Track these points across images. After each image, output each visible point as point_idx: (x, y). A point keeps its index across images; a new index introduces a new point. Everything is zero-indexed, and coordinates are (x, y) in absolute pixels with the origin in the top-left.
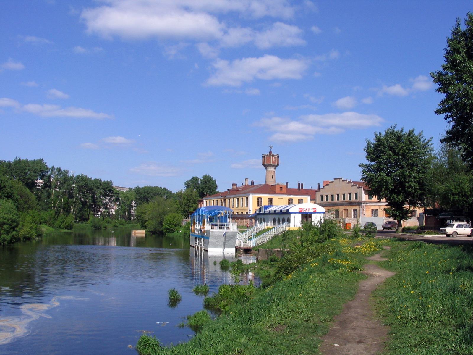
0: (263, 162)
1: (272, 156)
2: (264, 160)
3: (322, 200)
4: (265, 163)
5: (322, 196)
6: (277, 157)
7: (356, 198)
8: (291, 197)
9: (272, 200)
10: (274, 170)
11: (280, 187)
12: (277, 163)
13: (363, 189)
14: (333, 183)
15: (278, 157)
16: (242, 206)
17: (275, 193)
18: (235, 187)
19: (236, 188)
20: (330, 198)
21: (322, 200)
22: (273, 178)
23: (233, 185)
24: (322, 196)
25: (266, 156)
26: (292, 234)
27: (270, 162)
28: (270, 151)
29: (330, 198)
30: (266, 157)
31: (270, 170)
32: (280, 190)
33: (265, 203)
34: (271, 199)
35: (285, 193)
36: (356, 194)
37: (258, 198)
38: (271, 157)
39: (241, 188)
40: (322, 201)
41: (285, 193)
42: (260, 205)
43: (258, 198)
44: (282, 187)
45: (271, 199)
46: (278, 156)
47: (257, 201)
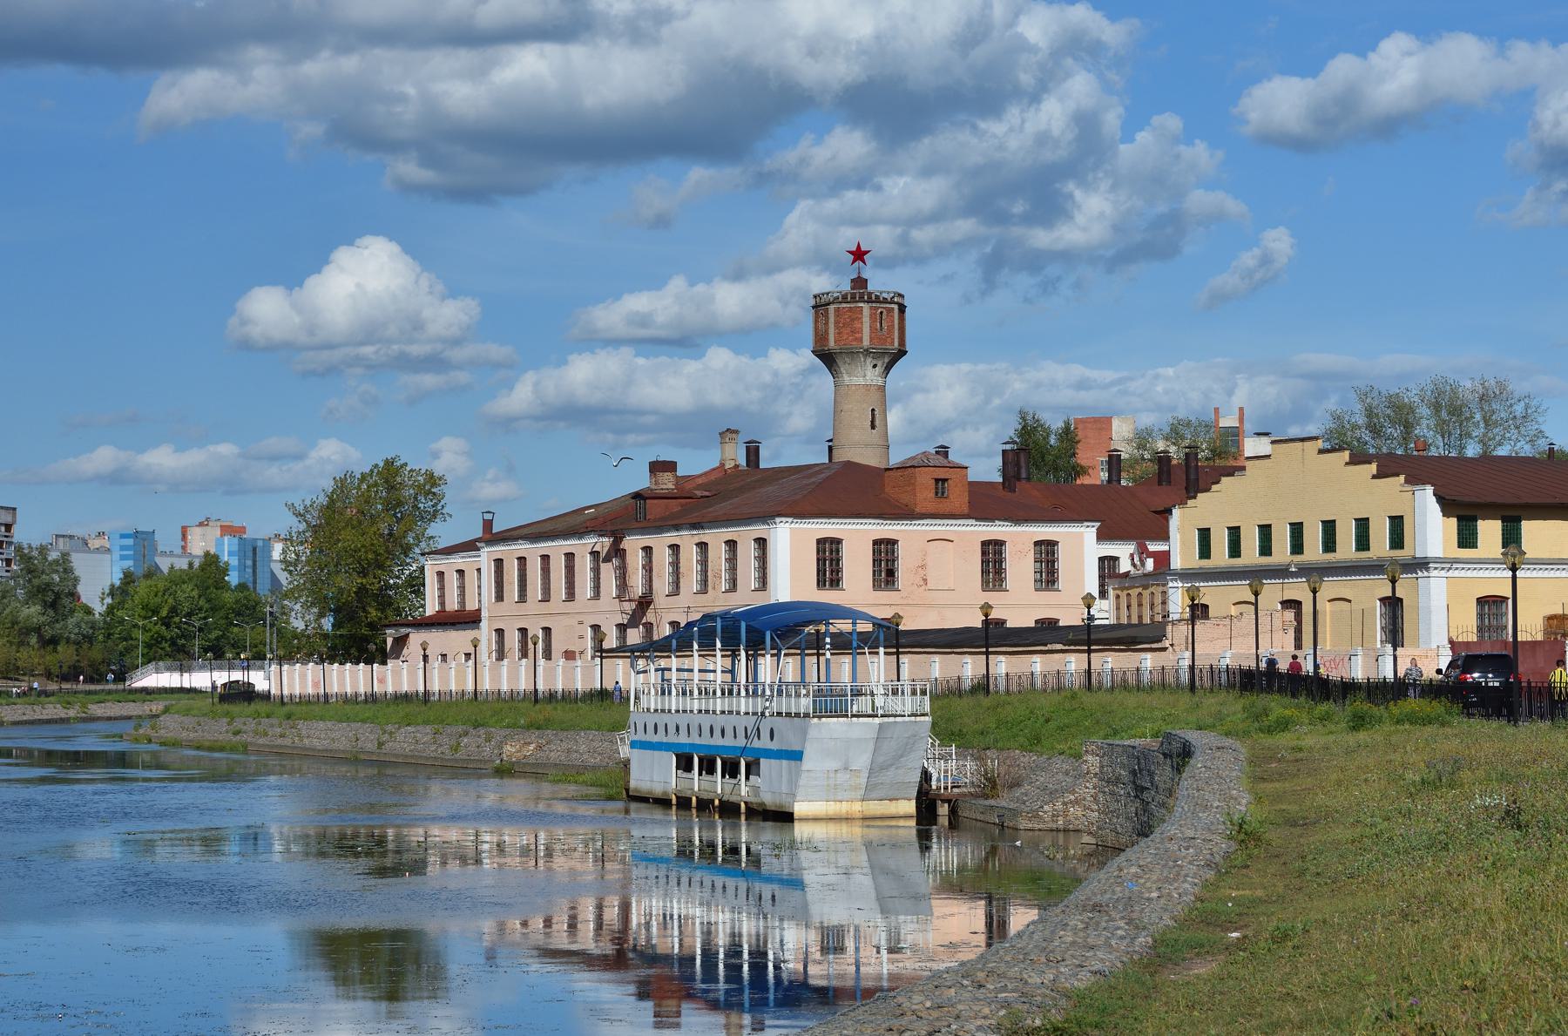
0: (820, 337)
1: (869, 301)
2: (827, 323)
3: (1205, 552)
4: (832, 343)
5: (1205, 534)
6: (896, 307)
7: (1397, 541)
8: (1265, 560)
9: (838, 551)
10: (880, 382)
11: (937, 480)
12: (896, 344)
13: (1440, 499)
14: (1266, 461)
15: (902, 309)
16: (546, 598)
17: (906, 513)
18: (667, 482)
19: (671, 486)
20: (1250, 542)
21: (1205, 552)
22: (873, 427)
23: (658, 467)
24: (1205, 534)
25: (835, 301)
26: (1076, 695)
27: (861, 340)
28: (855, 276)
29: (1250, 542)
30: (837, 310)
31: (861, 381)
32: (937, 493)
33: (1020, 566)
34: (836, 542)
35: (966, 510)
36: (1397, 523)
37: (821, 542)
38: (865, 307)
39: (700, 481)
40: (1208, 557)
41: (966, 510)
42: (832, 581)
43: (821, 542)
44: (944, 480)
45: (836, 542)
46: (900, 300)
47: (818, 560)
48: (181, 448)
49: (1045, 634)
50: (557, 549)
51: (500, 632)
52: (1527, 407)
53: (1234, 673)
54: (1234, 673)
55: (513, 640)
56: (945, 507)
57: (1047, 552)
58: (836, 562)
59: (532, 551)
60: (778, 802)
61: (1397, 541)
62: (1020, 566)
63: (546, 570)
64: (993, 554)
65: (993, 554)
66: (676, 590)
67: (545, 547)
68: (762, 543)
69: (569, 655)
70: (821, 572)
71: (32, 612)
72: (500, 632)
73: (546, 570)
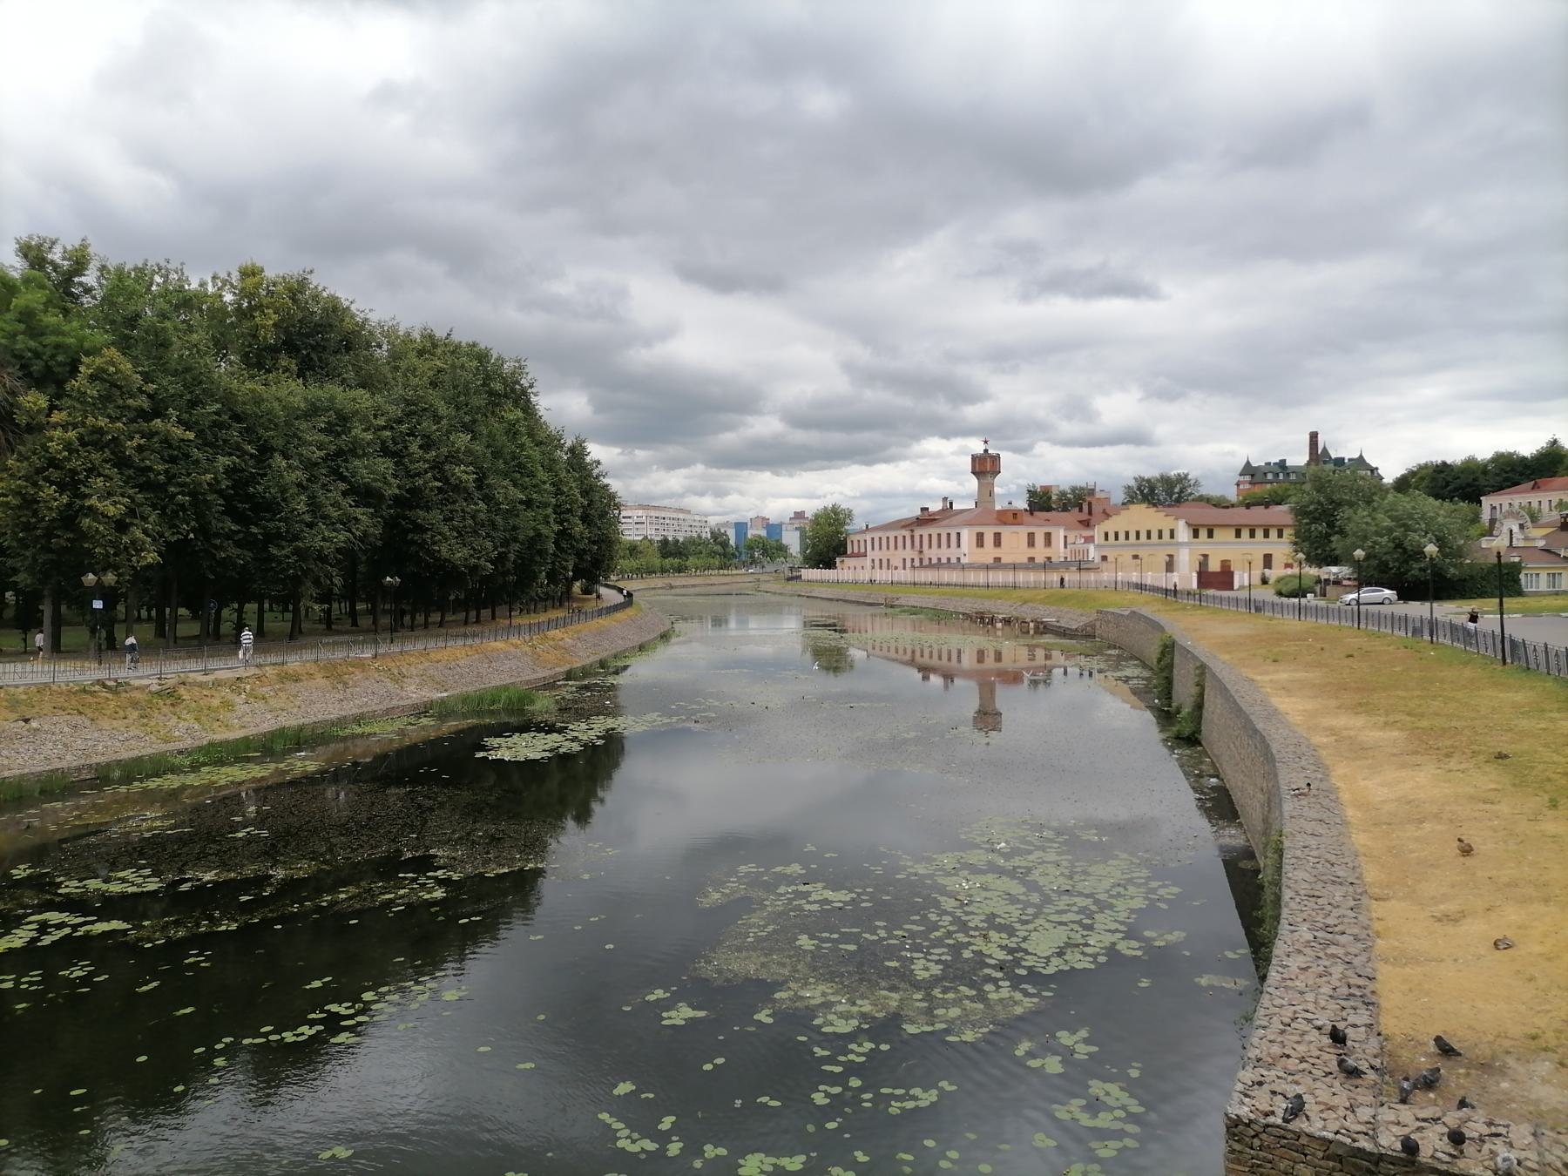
5: (1106, 535)
7: (1172, 536)
24: (1106, 535)
33: (1040, 540)
48: (647, 1097)
49: (1048, 565)
50: (892, 534)
51: (873, 560)
52: (440, 541)
53: (1557, 655)
54: (1557, 655)
55: (877, 563)
56: (1016, 521)
57: (1048, 536)
58: (1000, 539)
59: (883, 535)
60: (249, 263)
61: (1172, 536)
62: (1040, 540)
63: (888, 542)
64: (1031, 536)
65: (1031, 536)
66: (930, 547)
67: (888, 534)
68: (959, 534)
69: (896, 568)
70: (995, 542)
71: (718, 548)
72: (873, 560)
73: (888, 542)
